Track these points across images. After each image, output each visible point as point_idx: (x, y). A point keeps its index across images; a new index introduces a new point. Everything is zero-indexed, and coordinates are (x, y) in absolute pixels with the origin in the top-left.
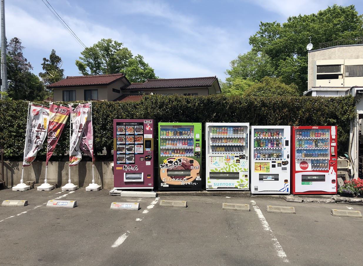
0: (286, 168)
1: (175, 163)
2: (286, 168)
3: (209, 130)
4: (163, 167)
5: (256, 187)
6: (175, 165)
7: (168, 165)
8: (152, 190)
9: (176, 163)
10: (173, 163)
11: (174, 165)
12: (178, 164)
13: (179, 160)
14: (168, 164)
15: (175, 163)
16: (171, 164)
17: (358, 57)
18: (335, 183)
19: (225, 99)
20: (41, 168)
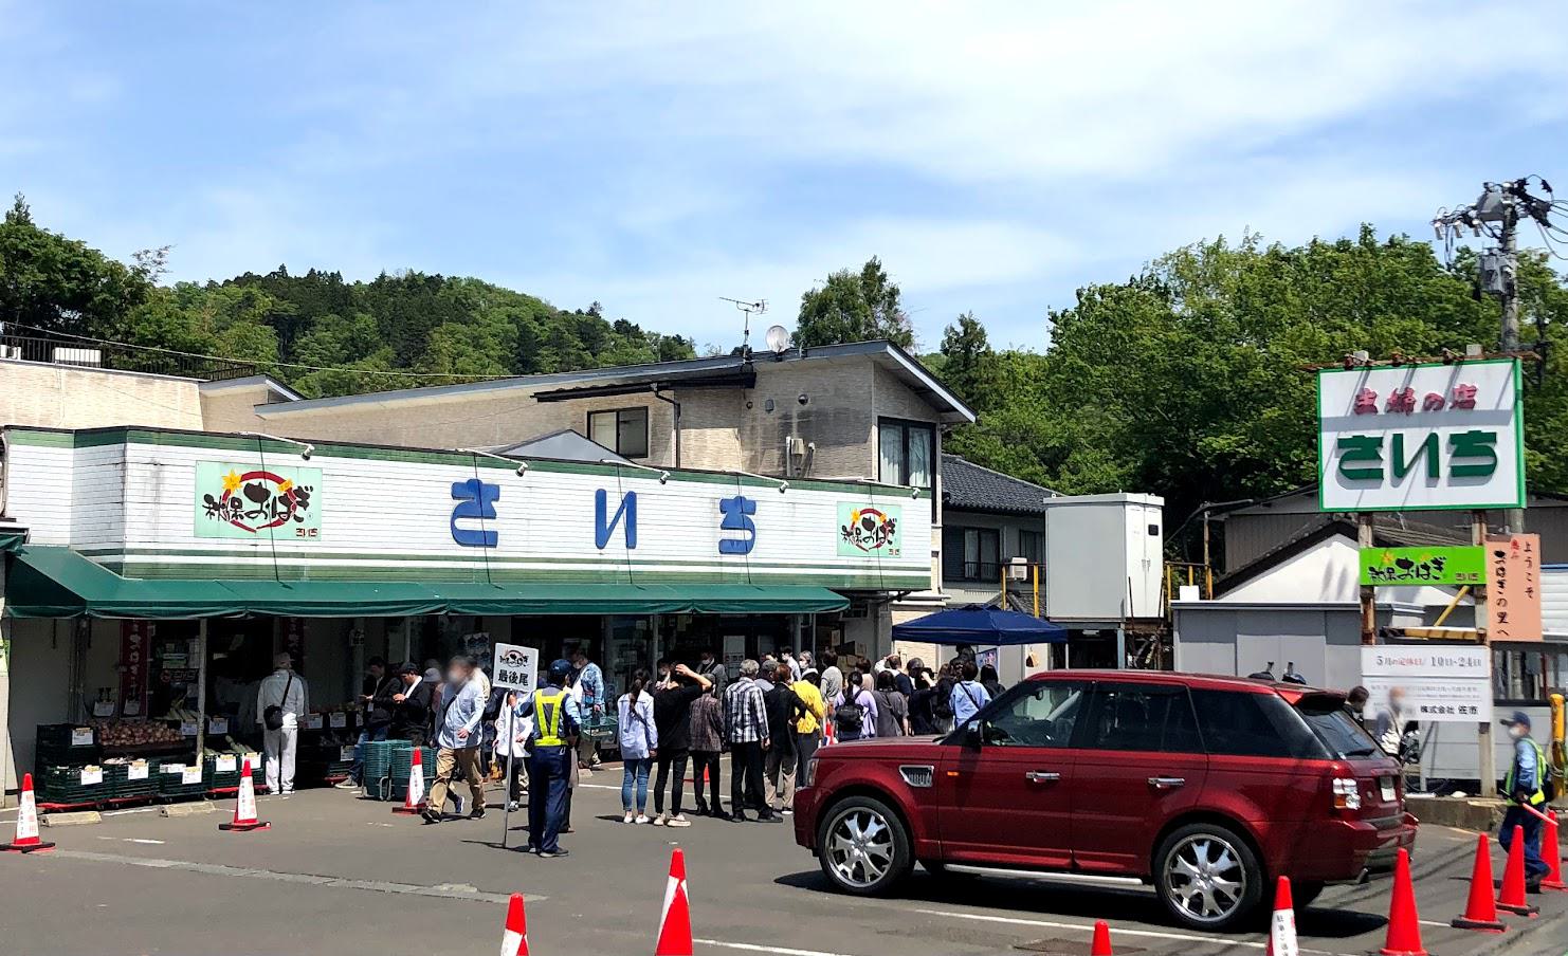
0: (494, 535)
1: (1420, 569)
2: (494, 535)
3: (94, 356)
4: (216, 513)
5: (1482, 632)
6: (1418, 575)
7: (240, 506)
8: (979, 676)
9: (1423, 571)
10: (1414, 568)
11: (1414, 574)
12: (1428, 574)
13: (1435, 562)
14: (1397, 568)
15: (1420, 569)
16: (1406, 571)
17: (248, 299)
18: (1197, 600)
19: (1217, 411)
20: (752, 808)
